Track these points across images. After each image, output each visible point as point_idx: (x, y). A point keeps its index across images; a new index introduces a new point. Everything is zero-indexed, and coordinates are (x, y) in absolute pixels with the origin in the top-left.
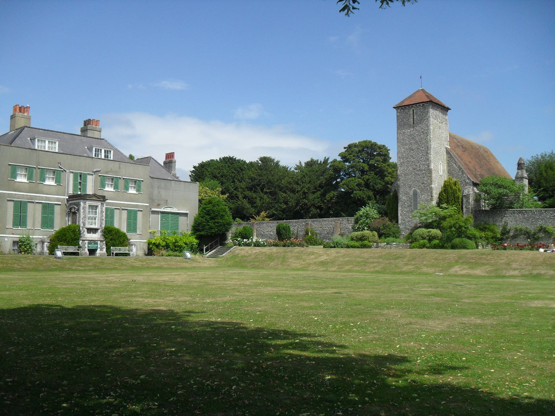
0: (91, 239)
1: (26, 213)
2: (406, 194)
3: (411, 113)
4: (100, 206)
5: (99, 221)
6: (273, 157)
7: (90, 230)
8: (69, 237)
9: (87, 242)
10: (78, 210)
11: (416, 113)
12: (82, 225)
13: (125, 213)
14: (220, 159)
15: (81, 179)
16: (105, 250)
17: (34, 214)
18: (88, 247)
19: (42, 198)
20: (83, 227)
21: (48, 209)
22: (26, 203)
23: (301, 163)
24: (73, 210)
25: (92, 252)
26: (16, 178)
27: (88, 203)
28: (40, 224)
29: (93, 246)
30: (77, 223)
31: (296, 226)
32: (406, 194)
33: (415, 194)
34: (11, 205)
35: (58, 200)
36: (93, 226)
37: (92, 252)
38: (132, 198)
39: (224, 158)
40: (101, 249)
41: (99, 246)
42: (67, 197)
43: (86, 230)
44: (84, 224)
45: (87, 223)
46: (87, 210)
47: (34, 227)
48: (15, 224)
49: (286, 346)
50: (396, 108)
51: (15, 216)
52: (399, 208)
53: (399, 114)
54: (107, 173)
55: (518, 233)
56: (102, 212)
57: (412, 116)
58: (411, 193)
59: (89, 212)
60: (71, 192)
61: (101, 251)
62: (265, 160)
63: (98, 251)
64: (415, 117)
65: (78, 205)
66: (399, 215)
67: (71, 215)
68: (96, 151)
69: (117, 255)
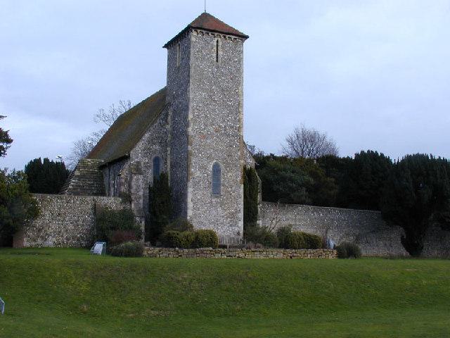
2: (203, 168)
32: (203, 168)
64: (220, 53)
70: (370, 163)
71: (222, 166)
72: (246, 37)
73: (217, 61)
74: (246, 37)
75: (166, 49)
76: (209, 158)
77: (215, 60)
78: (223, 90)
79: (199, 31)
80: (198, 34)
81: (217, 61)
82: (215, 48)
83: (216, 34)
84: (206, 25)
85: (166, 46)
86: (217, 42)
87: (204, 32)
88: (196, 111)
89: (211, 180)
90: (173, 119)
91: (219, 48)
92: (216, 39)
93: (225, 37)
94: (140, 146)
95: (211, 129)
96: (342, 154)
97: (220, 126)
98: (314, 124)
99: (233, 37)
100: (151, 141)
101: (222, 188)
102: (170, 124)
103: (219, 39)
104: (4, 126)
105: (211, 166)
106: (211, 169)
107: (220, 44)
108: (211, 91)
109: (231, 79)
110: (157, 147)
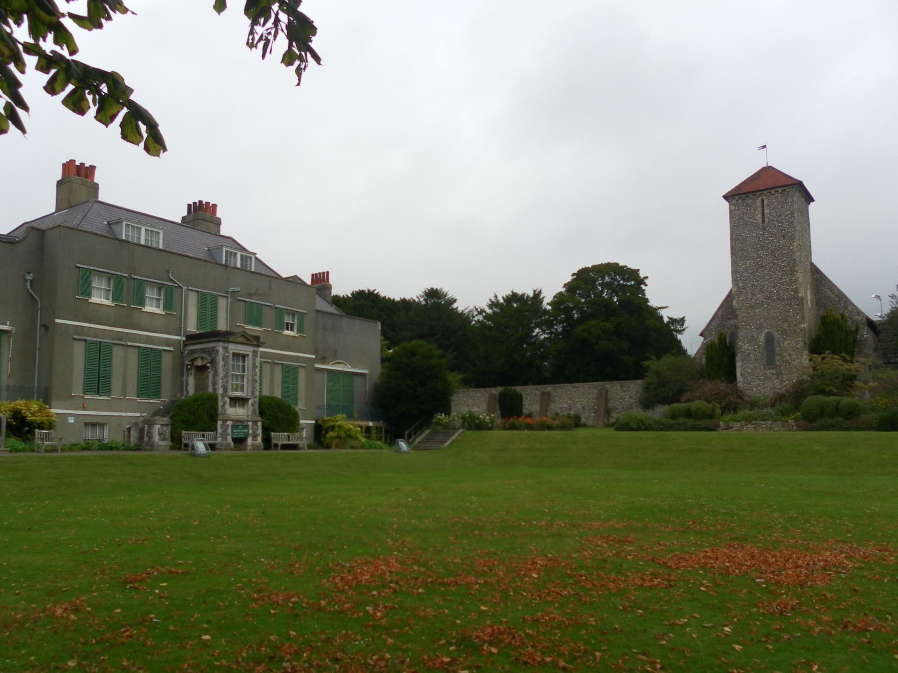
0: (236, 418)
1: (110, 366)
2: (753, 340)
3: (759, 204)
4: (251, 354)
5: (250, 383)
6: (445, 290)
7: (236, 401)
8: (196, 414)
9: (230, 423)
10: (213, 362)
11: (768, 205)
12: (220, 391)
13: (278, 369)
14: (352, 294)
15: (207, 306)
16: (260, 439)
17: (124, 368)
18: (233, 433)
19: (139, 338)
20: (223, 396)
21: (149, 359)
22: (109, 346)
23: (496, 297)
24: (199, 363)
25: (240, 441)
26: (90, 296)
27: (233, 348)
28: (135, 388)
29: (239, 433)
30: (210, 390)
31: (531, 397)
32: (753, 340)
33: (770, 339)
34: (79, 350)
35: (168, 342)
36: (238, 394)
37: (240, 441)
38: (289, 344)
39: (361, 293)
40: (255, 437)
41: (251, 432)
42: (184, 339)
43: (228, 400)
44: (225, 390)
45: (230, 387)
46: (231, 362)
47: (125, 396)
48: (86, 391)
49: (24, 451)
50: (726, 197)
51: (88, 372)
52: (739, 364)
53: (733, 208)
54: (250, 296)
55: (765, 405)
56: (254, 366)
57: (760, 209)
58: (762, 338)
59: (233, 366)
60: (192, 327)
61: (255, 440)
62: (433, 294)
63: (250, 440)
64: (767, 211)
65: (212, 352)
66: (738, 375)
67: (193, 371)
68: (226, 256)
69: (285, 447)
71: (776, 335)
76: (760, 328)
86: (763, 200)
87: (743, 196)
95: (760, 297)
107: (766, 202)
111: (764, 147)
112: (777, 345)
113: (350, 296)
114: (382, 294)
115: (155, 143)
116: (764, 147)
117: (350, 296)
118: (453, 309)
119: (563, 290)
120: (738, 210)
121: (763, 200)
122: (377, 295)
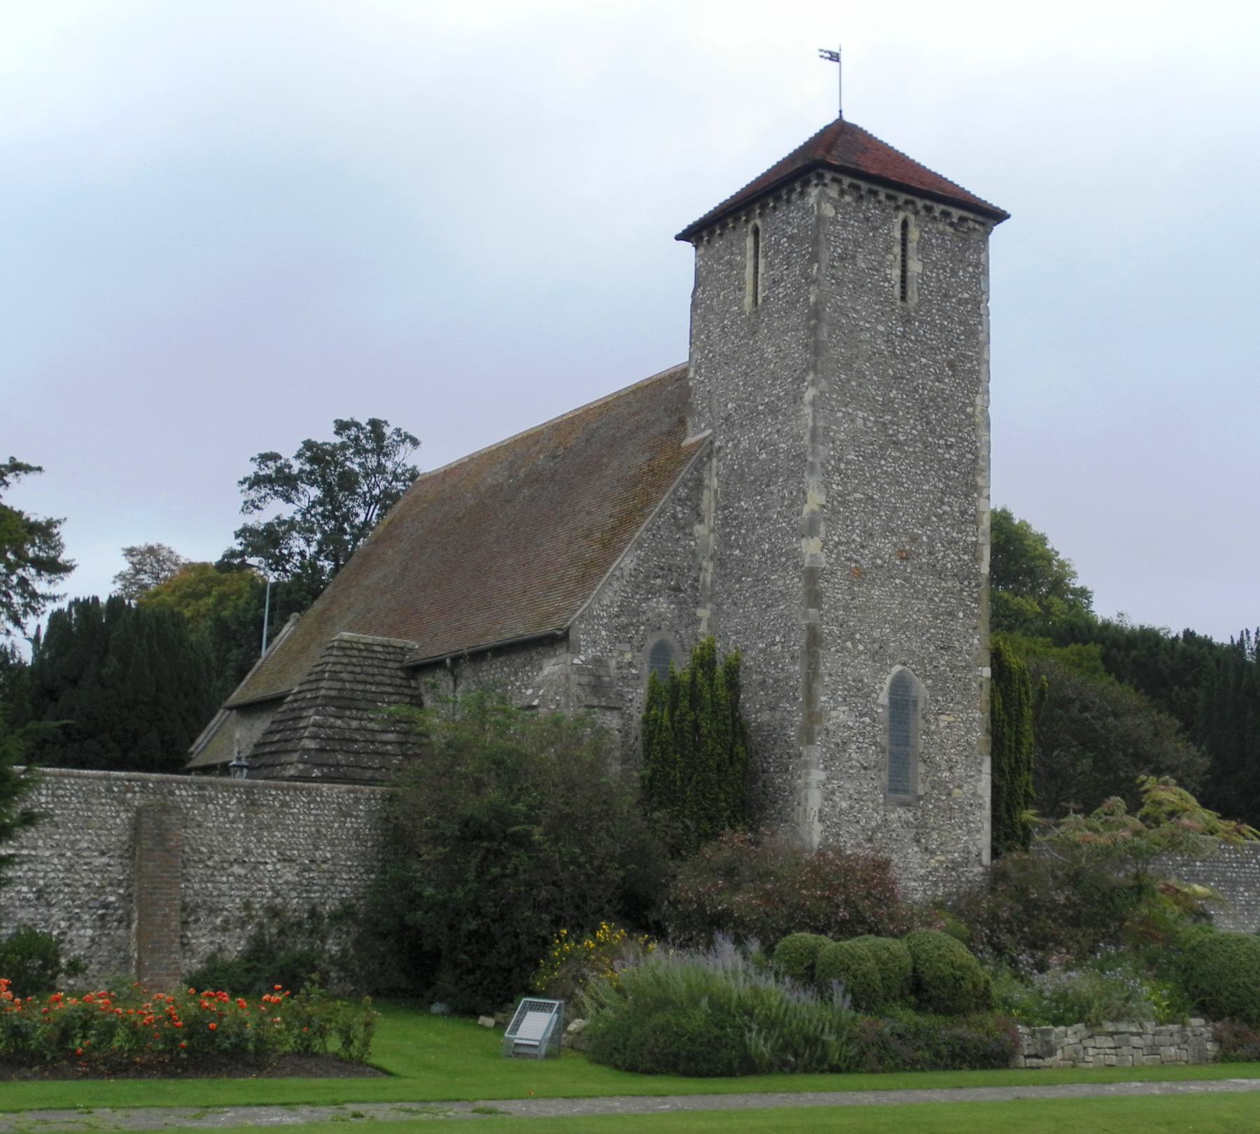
2: (859, 693)
32: (859, 693)
64: (915, 267)
70: (1148, 640)
71: (921, 689)
72: (999, 216)
73: (903, 298)
74: (999, 216)
75: (688, 248)
76: (879, 655)
77: (897, 291)
78: (923, 407)
79: (847, 181)
80: (842, 193)
81: (903, 298)
82: (897, 249)
83: (902, 197)
84: (841, 161)
85: (694, 234)
86: (905, 225)
87: (865, 186)
88: (837, 478)
89: (883, 739)
90: (726, 503)
91: (912, 246)
92: (901, 215)
93: (929, 209)
94: (607, 595)
95: (886, 547)
96: (1103, 609)
97: (914, 539)
98: (1010, 509)
99: (956, 213)
100: (642, 583)
101: (922, 769)
102: (710, 520)
103: (912, 218)
104: (24, 498)
105: (886, 687)
106: (884, 698)
107: (914, 234)
108: (888, 406)
109: (952, 365)
110: (663, 605)
111: (835, 57)
112: (922, 724)
113: (1100, 621)
114: (1222, 635)
115: (362, 1116)
116: (835, 57)
117: (1100, 621)
118: (37, 655)
119: (1048, 547)
120: (845, 226)
121: (905, 225)
122: (1206, 643)
